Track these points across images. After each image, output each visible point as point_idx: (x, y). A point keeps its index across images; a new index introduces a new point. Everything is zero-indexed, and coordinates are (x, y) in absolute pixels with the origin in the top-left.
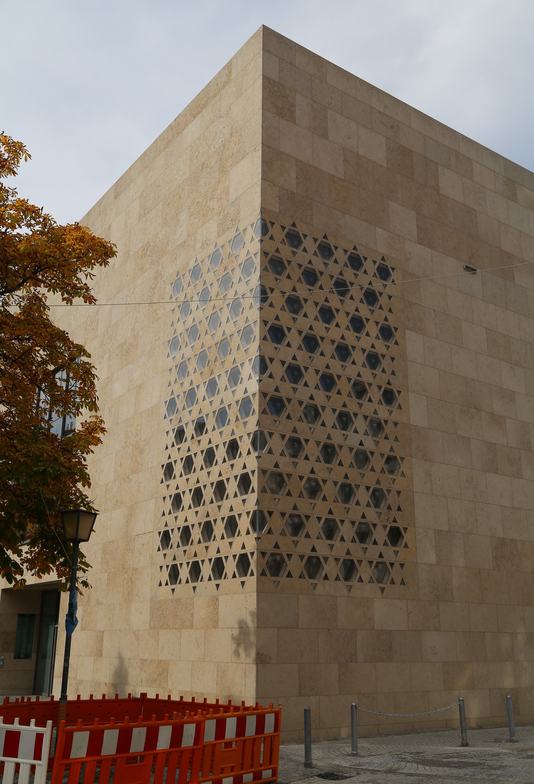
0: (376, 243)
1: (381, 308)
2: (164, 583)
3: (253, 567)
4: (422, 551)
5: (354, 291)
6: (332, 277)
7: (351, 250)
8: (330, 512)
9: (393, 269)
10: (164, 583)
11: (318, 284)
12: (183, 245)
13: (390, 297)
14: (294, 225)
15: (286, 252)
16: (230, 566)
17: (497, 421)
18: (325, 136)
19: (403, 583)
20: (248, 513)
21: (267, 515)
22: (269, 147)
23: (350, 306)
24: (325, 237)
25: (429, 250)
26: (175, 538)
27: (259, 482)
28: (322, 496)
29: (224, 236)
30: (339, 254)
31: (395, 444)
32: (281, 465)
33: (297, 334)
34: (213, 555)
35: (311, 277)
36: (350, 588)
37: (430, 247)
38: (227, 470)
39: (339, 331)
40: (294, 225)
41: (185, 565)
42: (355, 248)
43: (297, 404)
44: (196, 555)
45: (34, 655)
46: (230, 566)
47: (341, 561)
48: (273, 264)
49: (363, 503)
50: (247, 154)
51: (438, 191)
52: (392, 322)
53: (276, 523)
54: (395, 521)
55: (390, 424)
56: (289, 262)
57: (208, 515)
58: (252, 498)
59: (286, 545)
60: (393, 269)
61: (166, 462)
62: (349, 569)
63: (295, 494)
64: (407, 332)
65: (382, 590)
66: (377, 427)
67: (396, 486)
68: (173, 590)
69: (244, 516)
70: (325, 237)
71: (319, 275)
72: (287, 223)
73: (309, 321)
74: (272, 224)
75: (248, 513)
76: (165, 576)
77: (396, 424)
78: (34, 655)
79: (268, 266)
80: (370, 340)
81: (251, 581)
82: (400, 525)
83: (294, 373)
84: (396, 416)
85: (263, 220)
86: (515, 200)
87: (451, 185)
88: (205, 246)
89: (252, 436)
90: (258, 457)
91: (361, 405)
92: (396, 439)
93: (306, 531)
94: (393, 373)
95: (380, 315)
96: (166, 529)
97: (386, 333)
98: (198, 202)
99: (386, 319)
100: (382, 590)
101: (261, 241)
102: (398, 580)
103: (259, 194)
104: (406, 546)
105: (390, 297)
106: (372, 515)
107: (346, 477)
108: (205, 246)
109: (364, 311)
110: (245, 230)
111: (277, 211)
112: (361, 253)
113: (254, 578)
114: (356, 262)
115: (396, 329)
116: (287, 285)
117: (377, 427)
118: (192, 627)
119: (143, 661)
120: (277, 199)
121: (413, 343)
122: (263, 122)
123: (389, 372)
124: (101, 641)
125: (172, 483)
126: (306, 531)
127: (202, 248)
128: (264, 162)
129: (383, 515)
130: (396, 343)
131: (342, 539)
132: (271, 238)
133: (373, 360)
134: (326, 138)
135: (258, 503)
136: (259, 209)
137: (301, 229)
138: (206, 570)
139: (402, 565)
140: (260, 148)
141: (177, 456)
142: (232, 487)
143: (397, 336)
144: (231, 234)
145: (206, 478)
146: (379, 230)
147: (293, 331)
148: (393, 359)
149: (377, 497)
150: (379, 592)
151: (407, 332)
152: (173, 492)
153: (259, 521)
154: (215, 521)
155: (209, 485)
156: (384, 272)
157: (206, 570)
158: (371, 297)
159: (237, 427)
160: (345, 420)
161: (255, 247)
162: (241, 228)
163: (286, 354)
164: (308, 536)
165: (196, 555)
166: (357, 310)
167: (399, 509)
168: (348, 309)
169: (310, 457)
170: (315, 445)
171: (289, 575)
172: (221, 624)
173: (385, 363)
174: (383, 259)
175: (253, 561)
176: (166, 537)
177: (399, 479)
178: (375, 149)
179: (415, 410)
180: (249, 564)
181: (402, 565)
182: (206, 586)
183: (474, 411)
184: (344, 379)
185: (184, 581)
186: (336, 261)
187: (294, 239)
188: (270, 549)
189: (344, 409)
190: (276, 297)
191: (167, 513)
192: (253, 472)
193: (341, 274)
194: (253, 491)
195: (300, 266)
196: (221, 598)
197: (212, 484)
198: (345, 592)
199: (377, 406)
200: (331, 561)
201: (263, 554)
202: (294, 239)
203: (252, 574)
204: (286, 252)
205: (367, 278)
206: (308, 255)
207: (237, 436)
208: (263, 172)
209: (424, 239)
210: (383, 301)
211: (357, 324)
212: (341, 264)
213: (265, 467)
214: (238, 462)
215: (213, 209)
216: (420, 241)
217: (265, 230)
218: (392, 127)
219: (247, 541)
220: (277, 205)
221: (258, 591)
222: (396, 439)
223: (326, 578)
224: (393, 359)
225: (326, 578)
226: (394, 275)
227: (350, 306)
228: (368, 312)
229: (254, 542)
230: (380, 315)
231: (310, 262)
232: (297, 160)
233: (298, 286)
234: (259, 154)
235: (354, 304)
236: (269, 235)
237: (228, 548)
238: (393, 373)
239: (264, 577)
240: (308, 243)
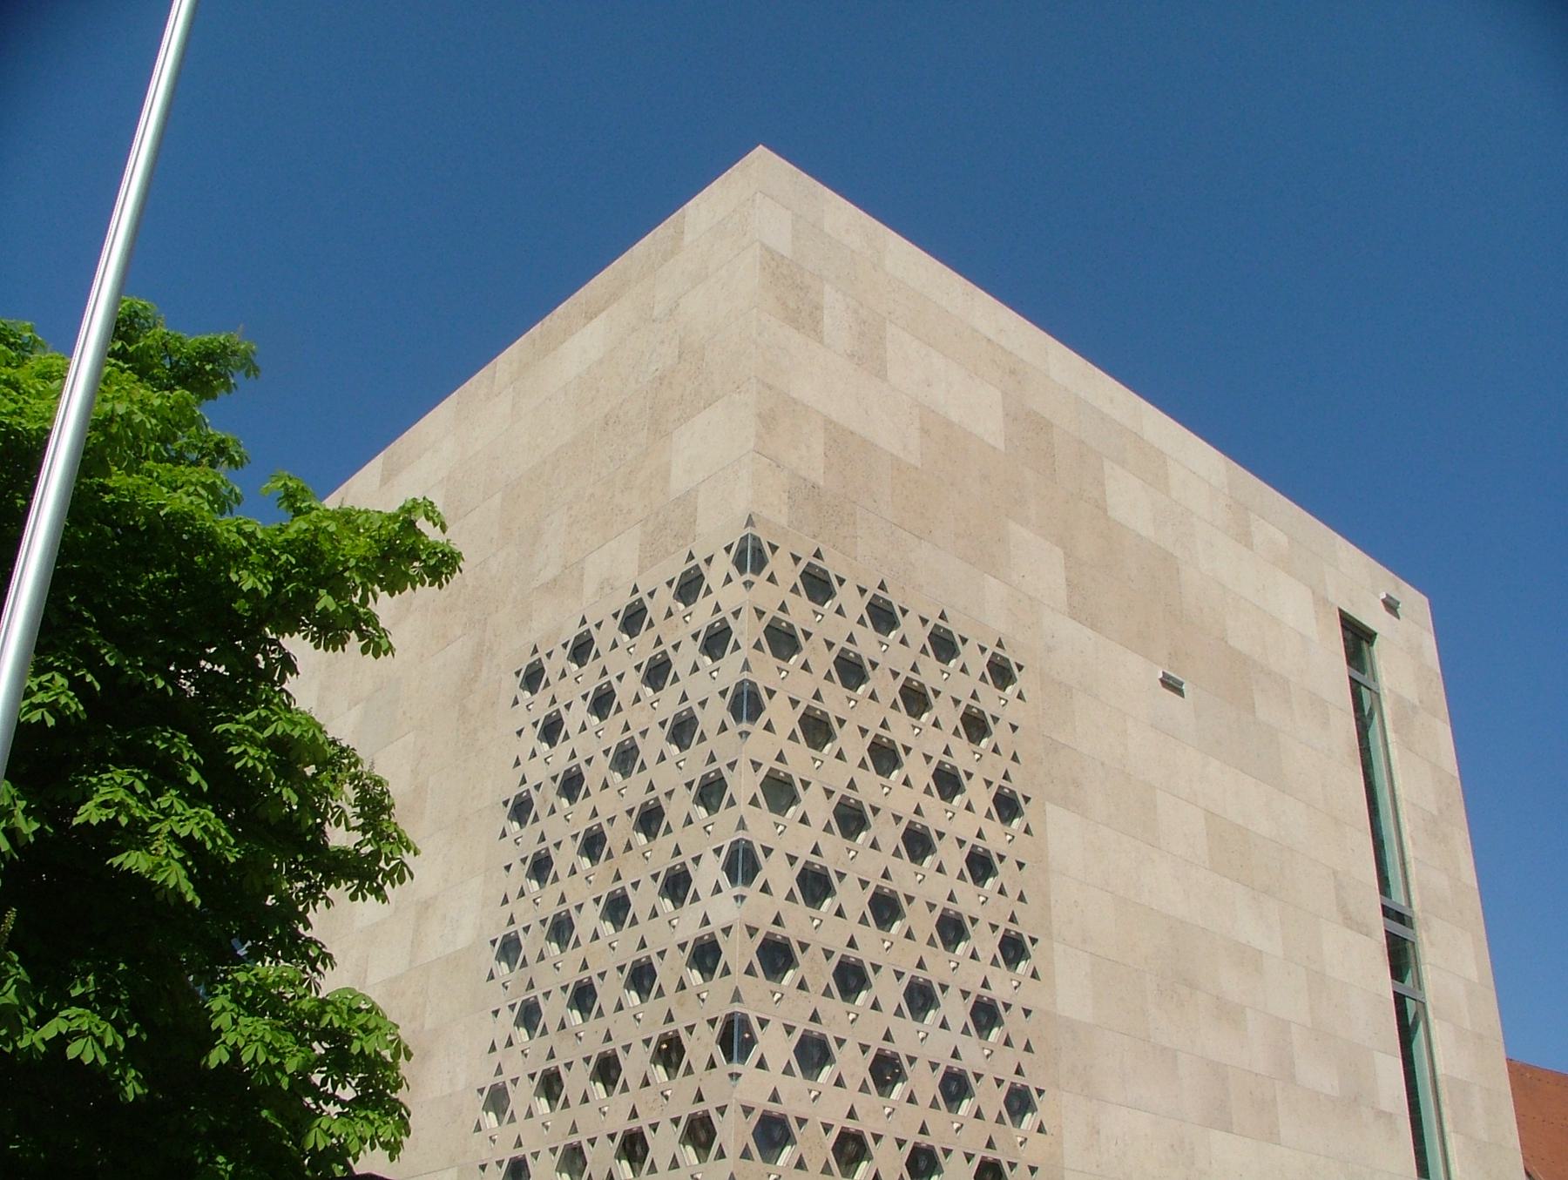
7: (934, 620)
12: (551, 587)
17: (1227, 1012)
18: (881, 374)
25: (1089, 632)
37: (1092, 627)
50: (719, 398)
52: (1018, 786)
64: (1049, 807)
70: (882, 587)
71: (868, 667)
86: (1249, 546)
88: (607, 590)
89: (719, 1025)
97: (1007, 806)
98: (592, 495)
108: (607, 590)
111: (784, 521)
120: (785, 496)
137: (832, 565)
141: (525, 1059)
151: (1049, 807)
156: (1001, 673)
159: (681, 1004)
169: (846, 1081)
174: (1000, 645)
179: (1063, 987)
207: (679, 1026)
209: (1081, 610)
210: (999, 733)
215: (629, 512)
220: (785, 509)
230: (993, 768)
232: (828, 422)
233: (827, 689)
238: (1021, 898)
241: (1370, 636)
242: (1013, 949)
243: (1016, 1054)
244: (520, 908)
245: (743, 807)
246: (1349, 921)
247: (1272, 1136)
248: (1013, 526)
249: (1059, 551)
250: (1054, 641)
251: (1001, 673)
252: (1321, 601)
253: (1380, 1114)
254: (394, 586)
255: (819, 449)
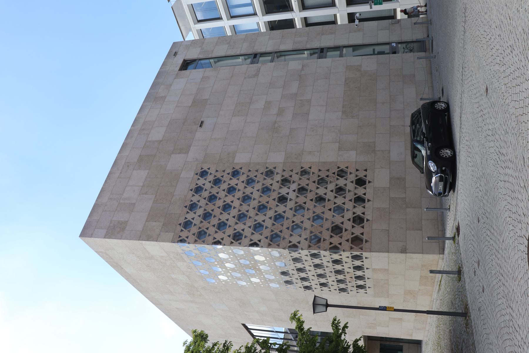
0: (188, 178)
1: (222, 177)
2: (366, 292)
3: (358, 253)
4: (350, 158)
5: (214, 191)
6: (207, 204)
8: (330, 210)
9: (202, 168)
10: (366, 292)
11: (211, 212)
13: (217, 171)
14: (180, 224)
15: (194, 230)
16: (358, 263)
19: (366, 170)
20: (331, 255)
21: (332, 245)
22: (140, 236)
23: (222, 194)
24: (186, 207)
25: (192, 147)
26: (342, 286)
27: (315, 250)
28: (322, 214)
29: (185, 259)
30: (195, 199)
31: (294, 172)
32: (306, 237)
33: (237, 225)
34: (352, 270)
35: (207, 216)
36: (369, 201)
38: (308, 263)
39: (235, 200)
40: (180, 224)
41: (356, 282)
42: (191, 190)
43: (274, 227)
44: (352, 278)
45: (401, 344)
46: (358, 263)
47: (355, 205)
48: (201, 237)
49: (325, 191)
51: (161, 141)
52: (230, 171)
53: (336, 240)
54: (334, 173)
55: (284, 174)
56: (200, 228)
57: (331, 272)
58: (323, 253)
59: (346, 235)
60: (202, 168)
61: (303, 289)
62: (359, 200)
63: (321, 229)
64: (235, 162)
65: (369, 182)
66: (285, 181)
67: (316, 171)
68: (367, 269)
69: (332, 256)
72: (180, 228)
73: (229, 217)
74: (180, 237)
75: (331, 255)
76: (362, 291)
77: (284, 170)
78: (401, 344)
79: (202, 240)
80: (239, 183)
81: (365, 254)
82: (336, 170)
83: (258, 227)
84: (279, 170)
85: (178, 242)
86: (165, 97)
87: (157, 134)
90: (302, 249)
91: (274, 190)
92: (292, 171)
93: (340, 224)
94: (257, 171)
95: (226, 178)
96: (338, 290)
97: (235, 174)
99: (228, 174)
100: (369, 182)
101: (189, 243)
102: (364, 173)
103: (164, 243)
104: (347, 168)
105: (217, 171)
106: (331, 187)
107: (312, 200)
109: (225, 186)
110: (183, 250)
112: (194, 186)
113: (364, 253)
114: (198, 190)
115: (234, 168)
116: (212, 230)
117: (285, 181)
118: (388, 280)
119: (404, 301)
121: (241, 159)
122: (127, 239)
123: (256, 174)
124: (394, 318)
125: (314, 286)
126: (340, 224)
127: (191, 269)
128: (148, 240)
129: (331, 180)
130: (241, 168)
131: (344, 203)
132: (187, 237)
133: (250, 182)
134: (135, 204)
135: (325, 250)
136: (173, 244)
137: (182, 220)
138: (359, 273)
139: (357, 170)
140: (141, 242)
141: (300, 284)
142: (317, 261)
143: (237, 168)
144: (184, 256)
145: (311, 273)
146: (182, 176)
147: (236, 227)
148: (250, 171)
149: (322, 181)
150: (370, 184)
151: (235, 162)
152: (319, 286)
153: (335, 249)
154: (334, 269)
155: (316, 271)
157: (359, 273)
158: (217, 182)
160: (282, 199)
161: (192, 246)
162: (182, 252)
163: (248, 232)
164: (342, 223)
165: (352, 278)
166: (224, 190)
167: (328, 170)
168: (224, 196)
170: (295, 217)
171: (362, 234)
172: (387, 268)
173: (252, 175)
175: (355, 253)
176: (342, 290)
177: (312, 170)
178: (139, 176)
179: (277, 159)
180: (357, 255)
181: (357, 170)
182: (367, 274)
183: (276, 125)
184: (261, 199)
185: (362, 263)
186: (199, 201)
187: (187, 224)
188: (349, 244)
189: (276, 200)
190: (219, 236)
191: (329, 289)
192: (309, 252)
193: (205, 199)
194: (319, 252)
195: (201, 222)
196: (373, 267)
197: (312, 259)
198: (370, 203)
199: (275, 181)
200: (355, 210)
201: (351, 248)
202: (187, 224)
203: (362, 254)
204: (194, 230)
205: (206, 183)
206: (196, 217)
208: (153, 240)
209: (185, 150)
210: (219, 175)
211: (231, 190)
212: (200, 198)
213: (307, 246)
214: (304, 258)
216: (187, 152)
217: (182, 241)
218: (128, 166)
219: (345, 256)
220: (170, 233)
221: (371, 252)
222: (292, 171)
223: (363, 213)
224: (250, 171)
225: (363, 213)
226: (205, 168)
227: (222, 194)
228: (225, 184)
229: (345, 253)
231: (199, 216)
232: (146, 221)
234: (144, 242)
235: (221, 191)
236: (186, 239)
237: (348, 264)
238: (257, 171)
239: (363, 248)
240: (190, 216)
241: (185, 61)
242: (270, 173)
243: (293, 174)
244: (332, 288)
245: (287, 209)
246: (256, 75)
247: (309, 101)
248: (167, 169)
249: (172, 155)
250: (195, 154)
251: (203, 174)
252: (177, 76)
253: (303, 69)
254: (303, 329)
255: (154, 223)
